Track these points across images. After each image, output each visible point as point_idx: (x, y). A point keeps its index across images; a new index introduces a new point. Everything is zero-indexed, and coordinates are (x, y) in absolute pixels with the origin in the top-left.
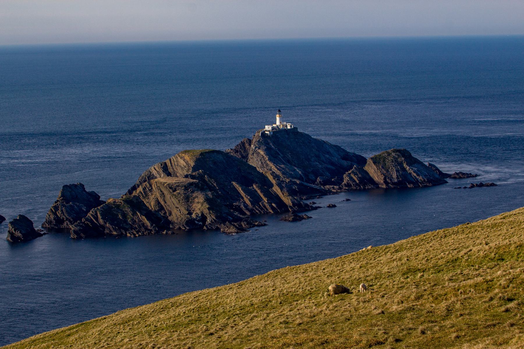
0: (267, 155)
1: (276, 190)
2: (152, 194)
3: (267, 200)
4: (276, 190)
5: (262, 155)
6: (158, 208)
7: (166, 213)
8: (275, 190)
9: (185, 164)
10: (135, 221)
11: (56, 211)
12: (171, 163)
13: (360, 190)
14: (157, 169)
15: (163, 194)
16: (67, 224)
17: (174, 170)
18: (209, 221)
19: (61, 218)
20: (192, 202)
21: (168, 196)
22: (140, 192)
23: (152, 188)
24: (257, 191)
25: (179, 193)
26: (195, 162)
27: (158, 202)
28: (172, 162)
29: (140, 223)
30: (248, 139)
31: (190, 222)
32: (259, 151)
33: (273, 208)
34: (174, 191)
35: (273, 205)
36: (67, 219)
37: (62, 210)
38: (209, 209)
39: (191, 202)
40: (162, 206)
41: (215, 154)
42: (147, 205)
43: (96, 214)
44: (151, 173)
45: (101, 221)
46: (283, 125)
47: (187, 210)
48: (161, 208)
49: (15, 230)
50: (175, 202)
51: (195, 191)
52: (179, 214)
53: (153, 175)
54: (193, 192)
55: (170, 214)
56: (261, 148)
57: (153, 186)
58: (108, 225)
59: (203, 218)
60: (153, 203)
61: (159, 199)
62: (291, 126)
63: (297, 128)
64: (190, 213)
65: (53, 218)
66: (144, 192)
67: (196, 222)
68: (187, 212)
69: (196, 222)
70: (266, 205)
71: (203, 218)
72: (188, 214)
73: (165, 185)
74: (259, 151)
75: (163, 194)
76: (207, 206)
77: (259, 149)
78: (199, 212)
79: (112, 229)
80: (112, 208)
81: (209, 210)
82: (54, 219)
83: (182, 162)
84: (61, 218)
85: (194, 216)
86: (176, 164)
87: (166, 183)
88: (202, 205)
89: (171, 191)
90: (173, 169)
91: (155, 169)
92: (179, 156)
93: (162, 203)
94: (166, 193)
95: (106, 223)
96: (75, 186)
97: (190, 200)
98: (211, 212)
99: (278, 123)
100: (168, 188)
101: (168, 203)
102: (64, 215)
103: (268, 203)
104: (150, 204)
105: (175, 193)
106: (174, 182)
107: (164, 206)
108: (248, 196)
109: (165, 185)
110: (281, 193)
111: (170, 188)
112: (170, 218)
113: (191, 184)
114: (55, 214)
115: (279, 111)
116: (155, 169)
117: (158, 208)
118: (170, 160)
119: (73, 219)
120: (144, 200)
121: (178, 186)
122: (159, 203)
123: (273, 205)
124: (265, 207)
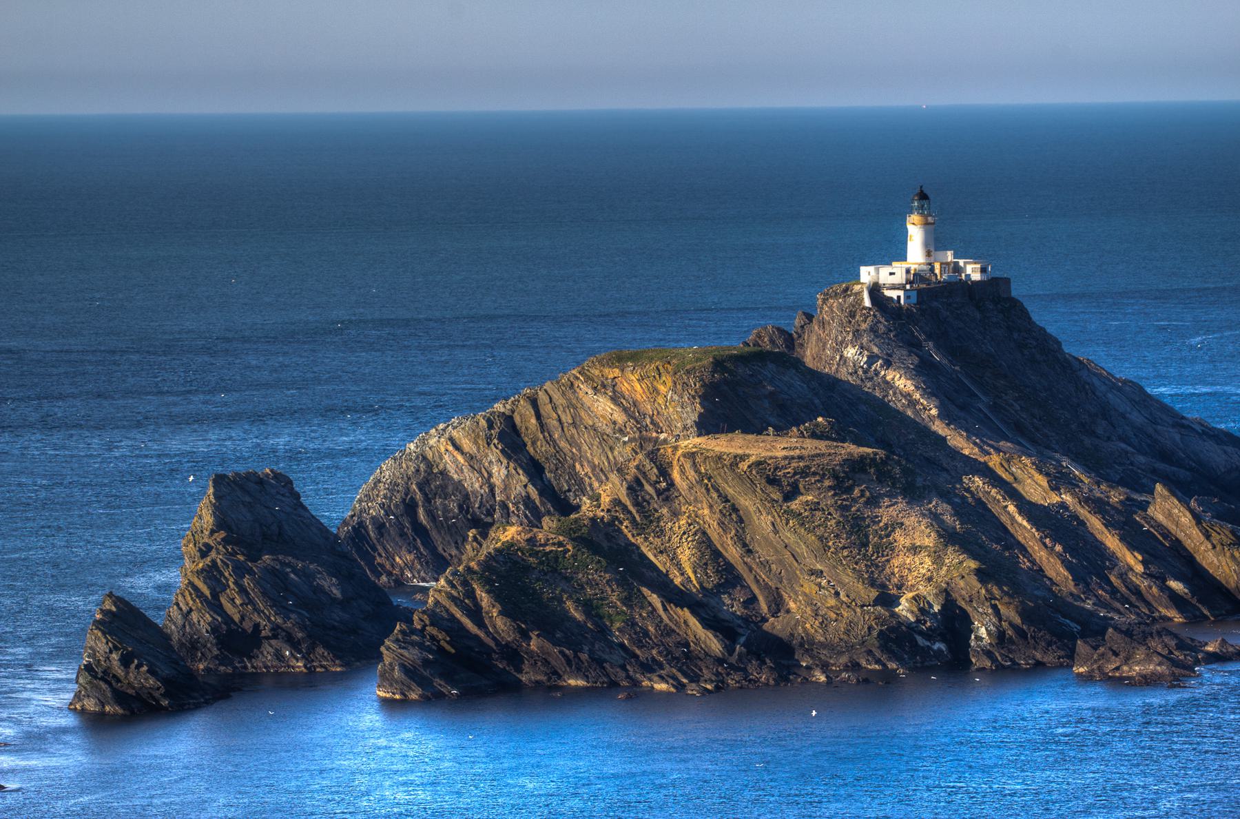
0: (930, 393)
1: (1169, 515)
2: (675, 514)
3: (1144, 562)
4: (1169, 515)
5: (908, 396)
6: (714, 579)
7: (753, 600)
8: (1160, 518)
9: (620, 417)
10: (646, 633)
11: (215, 595)
12: (538, 416)
13: (741, 688)
14: (467, 445)
15: (735, 509)
16: (279, 656)
17: (559, 450)
18: (983, 631)
19: (248, 626)
20: (886, 548)
21: (763, 522)
22: (617, 502)
23: (671, 484)
24: (1082, 523)
25: (815, 507)
26: (705, 398)
27: (709, 552)
28: (546, 409)
29: (670, 641)
30: (781, 331)
31: (897, 639)
32: (890, 375)
33: (1176, 600)
34: (788, 497)
35: (1175, 585)
36: (276, 629)
37: (242, 590)
38: (982, 575)
39: (878, 548)
40: (729, 568)
41: (771, 366)
42: (660, 562)
43: (471, 594)
44: (430, 466)
45: (500, 624)
46: (944, 265)
47: (872, 583)
48: (730, 578)
49: (126, 661)
50: (802, 549)
51: (881, 496)
52: (832, 602)
53: (444, 473)
54: (873, 502)
55: (777, 605)
56: (895, 358)
57: (676, 475)
58: (534, 644)
59: (953, 621)
60: (686, 555)
61: (714, 532)
62: (983, 270)
63: (1007, 281)
64: (888, 600)
65: (204, 628)
66: (636, 504)
67: (921, 641)
68: (874, 593)
69: (921, 641)
70: (1144, 584)
71: (953, 621)
72: (877, 602)
73: (744, 466)
74: (890, 375)
75: (732, 514)
76: (973, 564)
77: (888, 364)
78: (924, 589)
79: (558, 663)
80: (528, 569)
81: (982, 581)
82: (214, 630)
83: (603, 406)
84: (248, 626)
85: (904, 608)
86: (567, 419)
87: (743, 458)
88: (938, 560)
89: (777, 496)
90: (551, 441)
91: (458, 448)
92: (589, 379)
93: (733, 553)
94: (747, 503)
95: (525, 635)
96: (261, 481)
97: (873, 540)
98: (996, 592)
99: (916, 254)
100: (760, 483)
101: (763, 553)
102: (256, 609)
103: (1148, 575)
104: (674, 559)
105: (795, 505)
106: (780, 454)
107: (741, 568)
108: (1055, 540)
109: (744, 466)
110: (1195, 532)
111: (772, 481)
112: (776, 625)
113: (857, 467)
114: (214, 605)
115: (923, 196)
116: (458, 448)
117: (714, 579)
118: (534, 402)
119: (303, 628)
120: (639, 540)
121: (804, 473)
122: (717, 554)
123: (1175, 585)
124: (1137, 592)
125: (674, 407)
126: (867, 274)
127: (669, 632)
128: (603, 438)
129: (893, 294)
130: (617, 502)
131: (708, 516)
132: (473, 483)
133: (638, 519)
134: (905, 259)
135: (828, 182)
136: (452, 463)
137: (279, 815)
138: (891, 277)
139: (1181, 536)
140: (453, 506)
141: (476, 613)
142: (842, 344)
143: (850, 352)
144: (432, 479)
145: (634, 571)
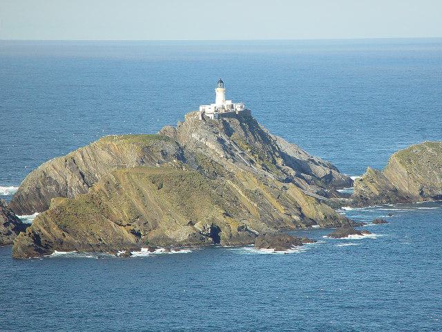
1: (294, 193)
9: (110, 158)
14: (58, 167)
22: (101, 190)
90: (86, 165)
93: (140, 208)
125: (132, 156)
126: (201, 108)
127: (116, 234)
128: (105, 165)
129: (210, 116)
130: (101, 190)
131: (133, 195)
132: (61, 181)
133: (229, 182)
134: (214, 103)
135: (184, 77)
136: (52, 174)
137: (48, 330)
138: (209, 110)
139: (298, 201)
140: (54, 188)
141: (48, 229)
142: (191, 132)
143: (194, 135)
144: (47, 179)
145: (105, 213)
